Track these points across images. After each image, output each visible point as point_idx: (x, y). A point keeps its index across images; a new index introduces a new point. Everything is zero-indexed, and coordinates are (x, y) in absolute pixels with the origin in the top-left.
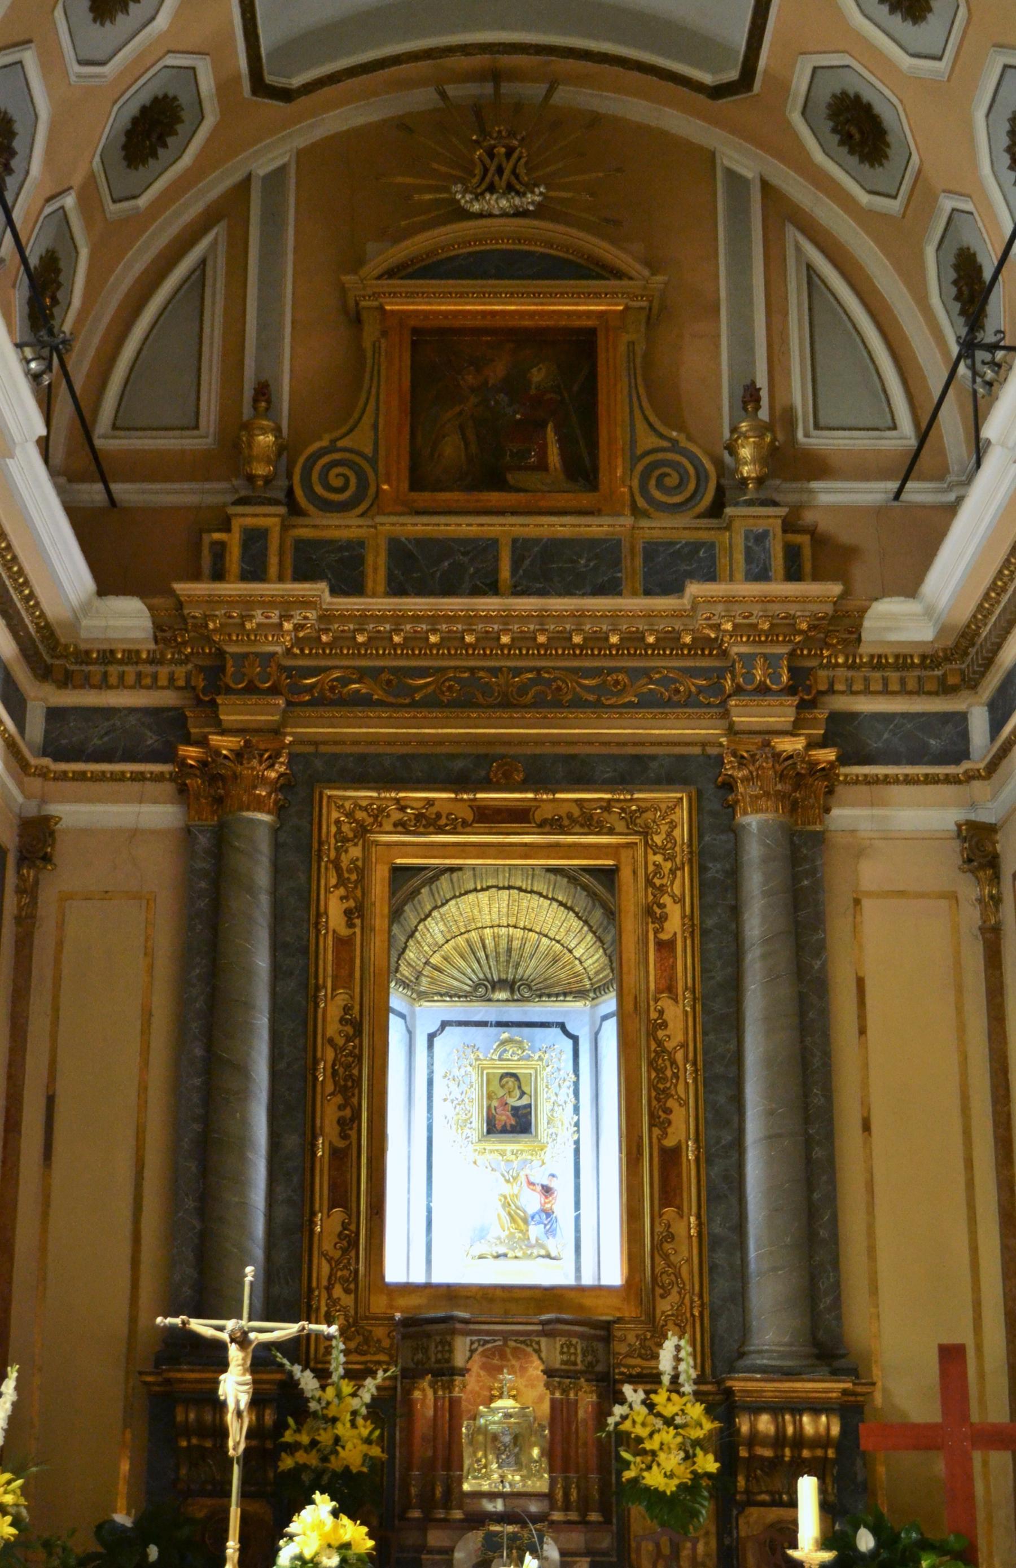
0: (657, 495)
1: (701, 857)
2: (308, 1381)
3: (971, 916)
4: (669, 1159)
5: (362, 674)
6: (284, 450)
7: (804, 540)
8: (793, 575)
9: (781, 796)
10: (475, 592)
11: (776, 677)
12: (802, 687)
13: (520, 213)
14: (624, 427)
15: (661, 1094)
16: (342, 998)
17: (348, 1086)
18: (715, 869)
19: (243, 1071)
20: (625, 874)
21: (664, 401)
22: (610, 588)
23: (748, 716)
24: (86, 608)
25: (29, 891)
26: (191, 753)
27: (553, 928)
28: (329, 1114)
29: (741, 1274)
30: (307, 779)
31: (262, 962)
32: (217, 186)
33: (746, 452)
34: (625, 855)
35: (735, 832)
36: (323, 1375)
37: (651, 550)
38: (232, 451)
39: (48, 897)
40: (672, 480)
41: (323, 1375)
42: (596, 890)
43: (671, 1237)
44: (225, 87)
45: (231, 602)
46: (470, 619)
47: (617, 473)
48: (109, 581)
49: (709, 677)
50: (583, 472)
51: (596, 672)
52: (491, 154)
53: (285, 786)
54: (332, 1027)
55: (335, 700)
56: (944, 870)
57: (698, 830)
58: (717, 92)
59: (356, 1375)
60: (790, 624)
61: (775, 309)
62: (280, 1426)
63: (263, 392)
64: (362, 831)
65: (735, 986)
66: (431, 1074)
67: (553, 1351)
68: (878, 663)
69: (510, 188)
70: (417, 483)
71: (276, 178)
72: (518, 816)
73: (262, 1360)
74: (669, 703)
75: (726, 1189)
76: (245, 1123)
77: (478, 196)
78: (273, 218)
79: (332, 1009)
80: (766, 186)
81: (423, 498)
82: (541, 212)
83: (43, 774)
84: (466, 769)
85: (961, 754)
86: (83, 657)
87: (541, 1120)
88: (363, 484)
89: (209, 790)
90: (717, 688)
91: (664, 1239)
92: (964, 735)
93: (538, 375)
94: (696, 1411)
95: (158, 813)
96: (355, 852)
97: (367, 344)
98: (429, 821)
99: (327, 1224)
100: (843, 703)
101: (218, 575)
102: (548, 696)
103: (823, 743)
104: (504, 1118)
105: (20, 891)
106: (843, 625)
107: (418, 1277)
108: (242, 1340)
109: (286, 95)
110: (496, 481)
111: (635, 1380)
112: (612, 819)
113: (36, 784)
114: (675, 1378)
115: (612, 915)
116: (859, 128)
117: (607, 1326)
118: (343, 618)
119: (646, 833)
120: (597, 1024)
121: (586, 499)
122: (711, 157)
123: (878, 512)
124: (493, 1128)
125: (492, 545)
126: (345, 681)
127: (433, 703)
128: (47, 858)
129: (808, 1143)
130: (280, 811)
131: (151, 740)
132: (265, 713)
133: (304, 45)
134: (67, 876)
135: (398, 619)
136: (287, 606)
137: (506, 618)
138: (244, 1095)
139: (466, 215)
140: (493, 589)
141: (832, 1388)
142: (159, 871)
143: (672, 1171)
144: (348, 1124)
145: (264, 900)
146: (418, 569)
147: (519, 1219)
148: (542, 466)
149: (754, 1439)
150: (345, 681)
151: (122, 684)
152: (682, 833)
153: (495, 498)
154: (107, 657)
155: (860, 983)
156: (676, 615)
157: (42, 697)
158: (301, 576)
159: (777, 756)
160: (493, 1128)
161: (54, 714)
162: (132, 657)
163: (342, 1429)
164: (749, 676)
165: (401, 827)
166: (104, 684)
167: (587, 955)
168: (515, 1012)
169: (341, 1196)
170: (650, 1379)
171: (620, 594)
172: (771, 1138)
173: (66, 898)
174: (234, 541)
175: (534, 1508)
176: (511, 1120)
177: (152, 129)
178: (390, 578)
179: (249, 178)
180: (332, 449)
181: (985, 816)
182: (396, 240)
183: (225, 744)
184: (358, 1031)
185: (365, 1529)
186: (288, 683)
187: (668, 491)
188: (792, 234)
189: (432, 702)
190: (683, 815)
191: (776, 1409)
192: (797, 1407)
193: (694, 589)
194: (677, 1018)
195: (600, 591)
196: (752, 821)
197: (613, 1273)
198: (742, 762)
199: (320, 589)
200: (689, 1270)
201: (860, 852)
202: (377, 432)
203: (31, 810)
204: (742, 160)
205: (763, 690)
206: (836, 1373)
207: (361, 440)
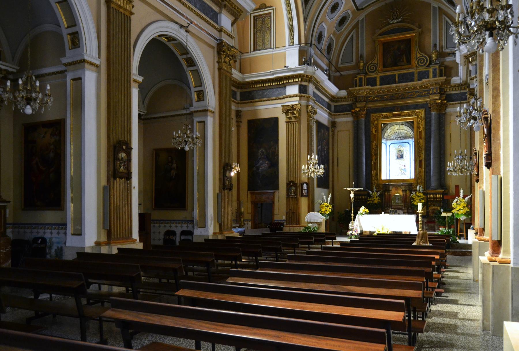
0: (420, 64)
2: (371, 192)
4: (420, 162)
5: (377, 97)
6: (365, 64)
7: (443, 68)
8: (441, 75)
9: (437, 109)
10: (392, 83)
11: (437, 91)
12: (441, 92)
13: (398, 22)
14: (416, 54)
15: (419, 152)
16: (375, 143)
17: (376, 155)
18: (428, 120)
19: (361, 153)
20: (415, 122)
21: (422, 48)
22: (412, 80)
23: (432, 98)
24: (338, 93)
25: (333, 131)
26: (353, 111)
27: (406, 130)
28: (373, 158)
29: (430, 176)
30: (369, 112)
31: (364, 139)
32: (354, 23)
33: (434, 56)
34: (415, 119)
35: (431, 114)
36: (373, 192)
37: (419, 73)
39: (336, 131)
40: (422, 61)
41: (373, 192)
42: (411, 124)
43: (420, 172)
44: (353, 12)
45: (357, 90)
46: (391, 87)
47: (414, 62)
48: (340, 89)
49: (427, 92)
50: (409, 61)
51: (411, 92)
52: (394, 13)
53: (366, 114)
54: (374, 147)
55: (373, 101)
59: (377, 192)
60: (438, 83)
61: (440, 29)
62: (367, 198)
64: (377, 119)
65: (430, 137)
66: (388, 151)
67: (403, 188)
68: (454, 86)
69: (397, 18)
70: (384, 66)
71: (363, 19)
72: (399, 115)
73: (355, 193)
74: (422, 96)
75: (428, 165)
76: (362, 160)
77: (392, 21)
78: (362, 27)
79: (373, 144)
80: (439, 8)
81: (385, 69)
82: (401, 22)
83: (334, 115)
84: (391, 109)
86: (338, 98)
87: (404, 156)
89: (356, 116)
90: (429, 93)
91: (419, 172)
93: (402, 47)
94: (422, 195)
95: (350, 119)
96: (376, 122)
97: (376, 46)
98: (386, 117)
99: (374, 173)
101: (356, 86)
102: (404, 97)
103: (445, 100)
104: (399, 156)
105: (332, 131)
106: (447, 82)
107: (388, 179)
108: (353, 190)
109: (363, 9)
110: (396, 65)
111: (414, 191)
112: (413, 114)
113: (333, 117)
114: (419, 190)
115: (413, 127)
117: (411, 184)
118: (373, 89)
119: (418, 116)
120: (411, 141)
121: (409, 66)
124: (398, 158)
125: (395, 75)
126: (374, 98)
127: (387, 100)
128: (335, 127)
129: (440, 158)
130: (366, 118)
131: (348, 108)
132: (363, 104)
133: (362, 3)
134: (339, 128)
135: (381, 89)
136: (365, 89)
137: (396, 87)
138: (362, 156)
139: (390, 24)
140: (395, 82)
141: (442, 191)
142: (350, 126)
143: (421, 162)
144: (376, 159)
145: (364, 130)
146: (385, 81)
147: (401, 170)
148: (403, 61)
149: (430, 198)
150: (374, 98)
151: (344, 101)
153: (395, 68)
154: (342, 98)
155: (450, 134)
156: (421, 83)
157: (333, 104)
158: (367, 85)
159: (436, 103)
160: (398, 158)
161: (335, 106)
162: (345, 98)
163: (375, 198)
164: (433, 91)
165: (383, 118)
166: (341, 102)
167: (410, 132)
168: (401, 141)
169: (375, 169)
170: (416, 191)
171: (414, 81)
172: (434, 158)
173: (338, 131)
174: (358, 79)
175: (401, 207)
176: (400, 157)
177: (342, 21)
178: (380, 82)
180: (371, 63)
182: (380, 29)
183: (357, 109)
184: (377, 146)
186: (366, 99)
187: (422, 63)
188: (443, 15)
190: (423, 113)
191: (433, 194)
192: (436, 194)
193: (423, 80)
194: (422, 141)
195: (411, 81)
196: (433, 113)
197: (413, 176)
198: (431, 104)
199: (370, 87)
200: (423, 176)
201: (451, 115)
202: (378, 60)
203: (333, 121)
205: (435, 93)
206: (442, 189)
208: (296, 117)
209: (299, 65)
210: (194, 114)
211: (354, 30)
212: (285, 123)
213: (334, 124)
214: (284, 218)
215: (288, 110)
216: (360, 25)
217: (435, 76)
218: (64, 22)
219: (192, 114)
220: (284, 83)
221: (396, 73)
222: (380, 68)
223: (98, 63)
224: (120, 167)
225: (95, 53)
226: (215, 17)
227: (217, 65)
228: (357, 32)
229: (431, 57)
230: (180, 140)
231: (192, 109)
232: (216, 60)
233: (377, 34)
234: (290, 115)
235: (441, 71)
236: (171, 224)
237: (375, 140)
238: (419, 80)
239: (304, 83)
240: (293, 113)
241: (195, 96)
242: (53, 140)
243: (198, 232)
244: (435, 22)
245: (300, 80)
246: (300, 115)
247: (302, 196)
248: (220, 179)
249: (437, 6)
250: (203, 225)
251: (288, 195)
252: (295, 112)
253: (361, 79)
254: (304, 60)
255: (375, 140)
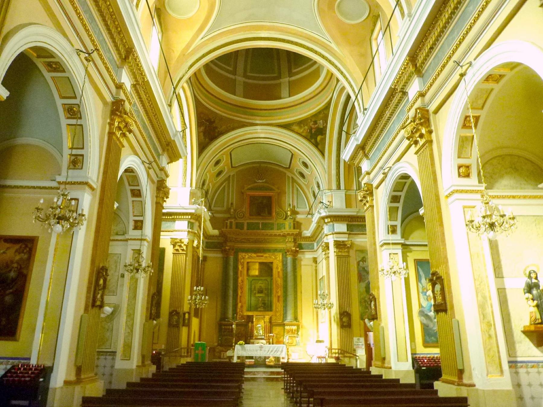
1: (283, 262)
3: (314, 268)
6: (235, 210)
8: (294, 228)
13: (263, 182)
18: (284, 263)
32: (227, 176)
35: (287, 258)
38: (228, 211)
56: (311, 262)
57: (283, 258)
58: (286, 168)
63: (232, 204)
70: (250, 215)
81: (252, 217)
85: (313, 248)
88: (244, 215)
92: (314, 246)
93: (265, 201)
96: (242, 260)
100: (299, 242)
106: (300, 234)
109: (235, 167)
116: (302, 175)
122: (285, 174)
123: (305, 219)
152: (281, 258)
177: (219, 174)
179: (230, 176)
181: (316, 256)
183: (227, 248)
185: (155, 372)
189: (253, 242)
202: (246, 209)
204: (290, 175)
207: (244, 210)
208: (183, 250)
209: (190, 204)
210: (130, 242)
211: (227, 182)
212: (172, 255)
213: (205, 258)
214: (163, 347)
215: (176, 243)
216: (231, 179)
217: (290, 228)
218: (67, 143)
219: (127, 240)
220: (174, 218)
221: (260, 222)
222: (247, 215)
223: (95, 187)
224: (98, 293)
225: (95, 178)
226: (159, 156)
227: (155, 199)
228: (229, 183)
229: (287, 214)
230: (132, 268)
231: (127, 237)
232: (155, 194)
233: (246, 188)
234: (177, 247)
235: (294, 224)
236: (106, 355)
237: (241, 276)
238: (278, 230)
239: (192, 221)
240: (180, 246)
241: (132, 224)
242: (18, 258)
243: (120, 364)
244: (289, 188)
245: (190, 217)
246: (187, 247)
247: (183, 325)
248: (147, 309)
249: (290, 176)
250: (127, 357)
251: (170, 325)
252: (182, 245)
253: (231, 223)
254: (193, 200)
255: (241, 276)
